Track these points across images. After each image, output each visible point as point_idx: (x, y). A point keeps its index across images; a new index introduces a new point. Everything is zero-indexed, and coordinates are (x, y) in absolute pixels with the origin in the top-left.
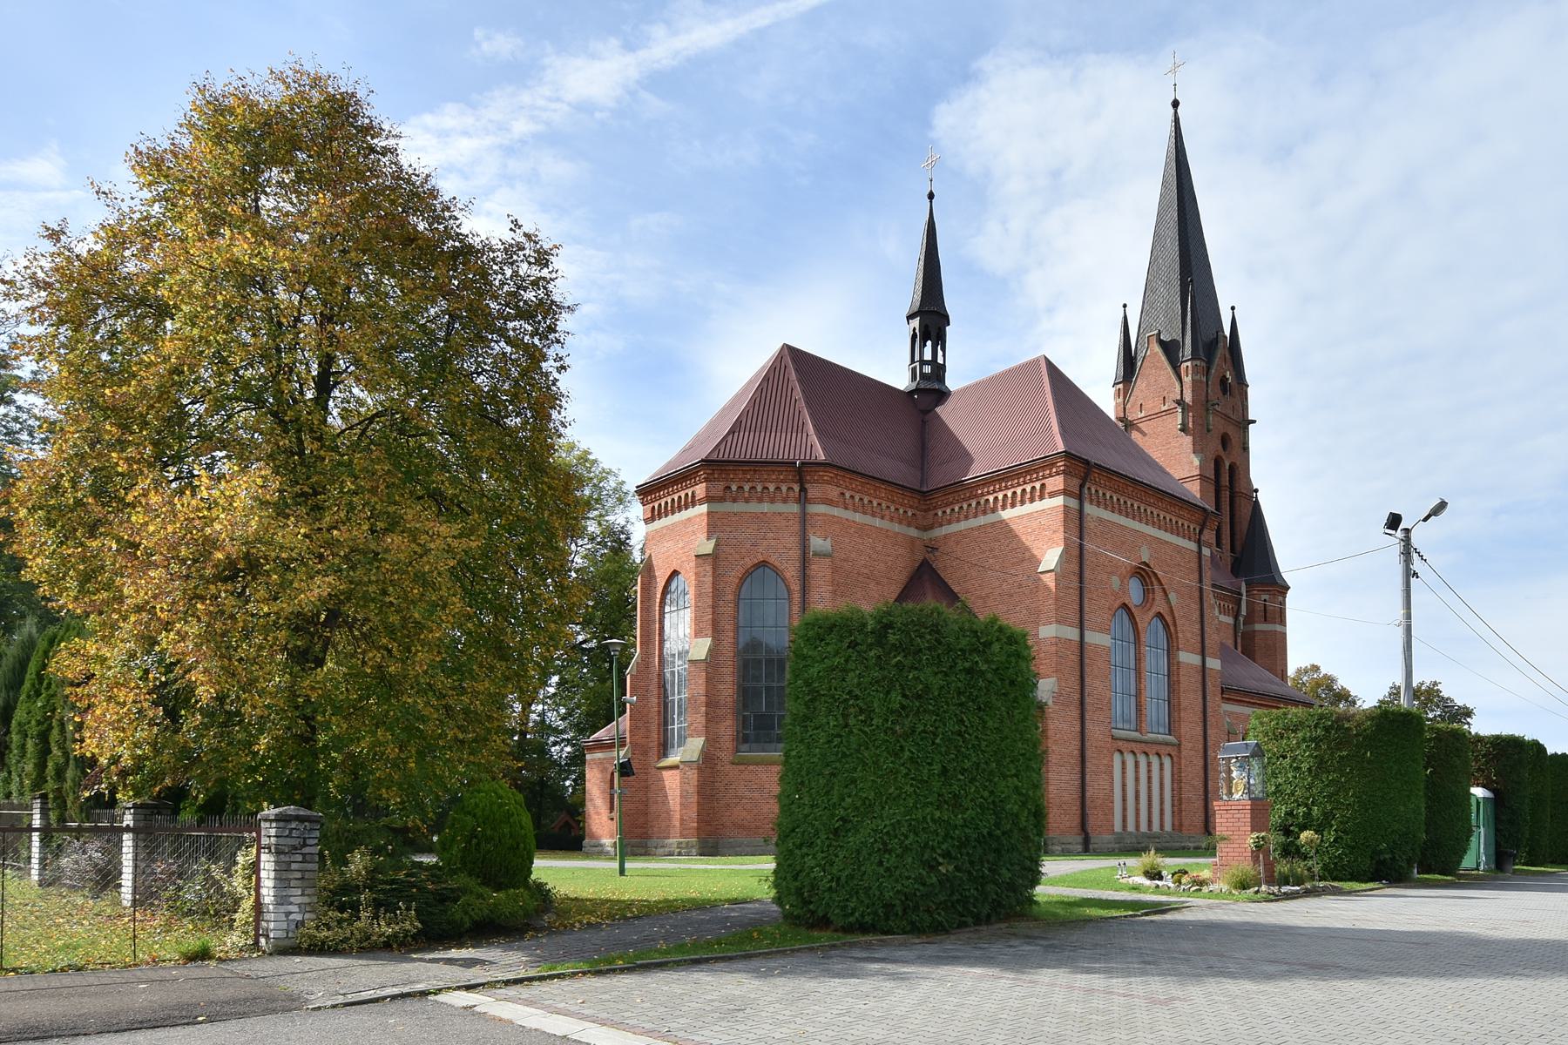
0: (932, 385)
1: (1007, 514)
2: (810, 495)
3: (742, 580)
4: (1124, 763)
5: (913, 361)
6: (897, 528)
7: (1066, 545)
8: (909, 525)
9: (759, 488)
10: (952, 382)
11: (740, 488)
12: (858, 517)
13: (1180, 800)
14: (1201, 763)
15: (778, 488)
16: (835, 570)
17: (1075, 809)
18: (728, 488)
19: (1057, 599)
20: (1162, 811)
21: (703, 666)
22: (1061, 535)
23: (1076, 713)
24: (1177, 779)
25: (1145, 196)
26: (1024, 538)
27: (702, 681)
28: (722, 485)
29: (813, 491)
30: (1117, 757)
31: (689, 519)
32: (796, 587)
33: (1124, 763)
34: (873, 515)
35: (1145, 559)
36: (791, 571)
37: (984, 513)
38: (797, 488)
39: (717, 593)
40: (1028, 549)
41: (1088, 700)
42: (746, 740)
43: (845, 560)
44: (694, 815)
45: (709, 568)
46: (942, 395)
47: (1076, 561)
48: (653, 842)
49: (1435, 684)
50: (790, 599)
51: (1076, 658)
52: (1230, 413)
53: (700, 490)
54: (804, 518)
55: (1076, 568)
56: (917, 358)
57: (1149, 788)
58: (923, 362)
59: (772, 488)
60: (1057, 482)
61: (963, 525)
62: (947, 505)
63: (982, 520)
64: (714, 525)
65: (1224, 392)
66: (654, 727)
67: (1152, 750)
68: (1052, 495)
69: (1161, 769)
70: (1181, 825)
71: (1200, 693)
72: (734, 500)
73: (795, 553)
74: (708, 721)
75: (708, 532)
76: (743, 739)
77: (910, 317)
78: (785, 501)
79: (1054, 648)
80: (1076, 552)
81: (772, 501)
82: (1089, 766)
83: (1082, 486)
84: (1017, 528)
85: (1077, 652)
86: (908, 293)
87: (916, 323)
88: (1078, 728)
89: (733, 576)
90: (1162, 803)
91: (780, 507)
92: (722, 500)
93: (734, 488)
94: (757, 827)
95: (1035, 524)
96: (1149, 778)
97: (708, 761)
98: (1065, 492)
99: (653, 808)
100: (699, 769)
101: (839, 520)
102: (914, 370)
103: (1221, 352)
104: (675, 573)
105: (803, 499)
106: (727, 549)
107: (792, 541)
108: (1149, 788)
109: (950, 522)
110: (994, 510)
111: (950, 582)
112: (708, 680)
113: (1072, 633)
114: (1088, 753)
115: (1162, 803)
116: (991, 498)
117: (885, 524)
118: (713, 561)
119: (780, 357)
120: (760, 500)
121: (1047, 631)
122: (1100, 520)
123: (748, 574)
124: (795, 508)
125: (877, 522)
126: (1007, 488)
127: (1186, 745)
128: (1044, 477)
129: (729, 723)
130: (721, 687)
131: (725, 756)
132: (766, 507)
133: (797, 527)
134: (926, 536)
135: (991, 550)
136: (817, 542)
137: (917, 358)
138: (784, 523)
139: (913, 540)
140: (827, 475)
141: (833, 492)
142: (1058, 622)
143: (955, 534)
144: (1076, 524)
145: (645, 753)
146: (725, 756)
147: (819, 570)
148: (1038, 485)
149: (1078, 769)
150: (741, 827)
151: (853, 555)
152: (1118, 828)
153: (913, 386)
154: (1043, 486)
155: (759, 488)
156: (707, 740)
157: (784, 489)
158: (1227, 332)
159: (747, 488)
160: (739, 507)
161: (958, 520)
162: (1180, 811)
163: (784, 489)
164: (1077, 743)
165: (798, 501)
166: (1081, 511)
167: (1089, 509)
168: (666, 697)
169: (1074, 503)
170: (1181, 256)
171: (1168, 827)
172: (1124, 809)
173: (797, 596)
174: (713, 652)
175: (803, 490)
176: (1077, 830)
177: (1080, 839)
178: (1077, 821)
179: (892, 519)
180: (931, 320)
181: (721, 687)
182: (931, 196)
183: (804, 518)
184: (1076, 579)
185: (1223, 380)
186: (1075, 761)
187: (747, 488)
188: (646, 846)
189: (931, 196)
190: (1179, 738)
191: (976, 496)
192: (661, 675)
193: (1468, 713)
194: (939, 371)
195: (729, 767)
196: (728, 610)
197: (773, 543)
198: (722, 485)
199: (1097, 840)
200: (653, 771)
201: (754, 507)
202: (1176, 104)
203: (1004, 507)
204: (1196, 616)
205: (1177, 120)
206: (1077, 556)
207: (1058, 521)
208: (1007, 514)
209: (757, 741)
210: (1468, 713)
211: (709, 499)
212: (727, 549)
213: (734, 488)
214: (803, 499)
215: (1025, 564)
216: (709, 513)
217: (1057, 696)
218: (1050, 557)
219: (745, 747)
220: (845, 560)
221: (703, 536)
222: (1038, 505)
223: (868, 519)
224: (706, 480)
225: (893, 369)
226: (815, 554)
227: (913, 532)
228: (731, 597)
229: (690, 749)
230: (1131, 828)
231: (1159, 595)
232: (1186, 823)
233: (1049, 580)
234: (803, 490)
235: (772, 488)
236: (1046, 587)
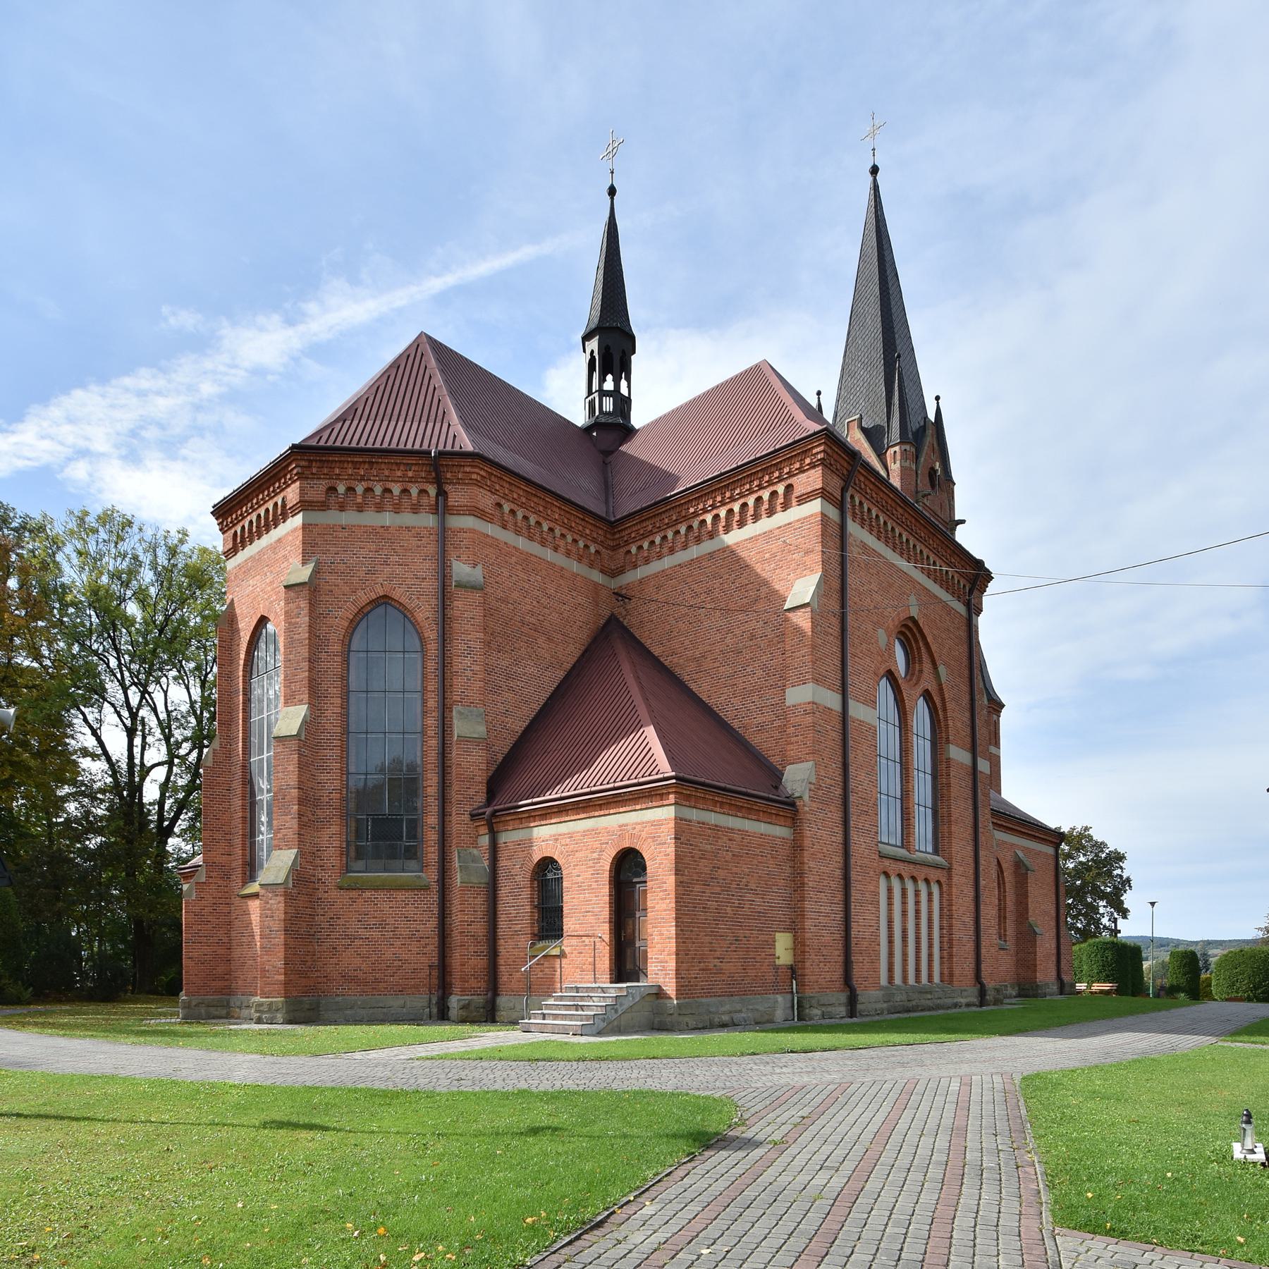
0: (613, 426)
1: (732, 538)
2: (452, 501)
3: (354, 625)
4: (890, 890)
5: (590, 392)
6: (575, 567)
7: (825, 571)
8: (591, 566)
9: (378, 490)
10: (638, 419)
11: (351, 489)
12: (521, 543)
13: (950, 941)
14: (972, 894)
15: (405, 491)
16: (488, 612)
17: (837, 955)
18: (332, 489)
19: (814, 647)
20: (930, 955)
21: (294, 745)
22: (817, 557)
23: (837, 816)
24: (947, 913)
25: (846, 252)
26: (758, 568)
27: (292, 767)
28: (323, 485)
29: (457, 496)
30: (882, 880)
31: (279, 540)
32: (431, 634)
33: (890, 890)
34: (543, 543)
35: (914, 612)
36: (425, 612)
37: (698, 540)
38: (432, 491)
39: (316, 642)
40: (765, 583)
41: (852, 798)
42: (360, 854)
43: (505, 601)
44: (280, 964)
45: (304, 604)
46: (628, 432)
47: (836, 596)
48: (235, 1001)
49: (1086, 829)
50: (423, 651)
51: (836, 736)
52: (937, 509)
53: (292, 494)
54: (443, 536)
55: (836, 607)
56: (595, 387)
57: (917, 925)
58: (603, 393)
59: (396, 489)
60: (812, 479)
61: (667, 562)
62: (644, 537)
63: (695, 551)
64: (311, 543)
65: (933, 486)
66: (238, 841)
67: (921, 873)
68: (803, 499)
69: (930, 900)
70: (951, 975)
71: (970, 802)
72: (342, 508)
73: (431, 586)
74: (302, 825)
75: (304, 553)
76: (356, 852)
77: (586, 338)
78: (415, 509)
79: (809, 719)
80: (836, 584)
81: (397, 509)
82: (855, 895)
83: (844, 490)
84: (748, 555)
85: (839, 727)
86: (583, 305)
87: (593, 345)
88: (840, 838)
89: (340, 617)
90: (930, 946)
91: (407, 519)
92: (323, 506)
93: (341, 489)
94: (377, 981)
95: (775, 546)
96: (917, 912)
97: (301, 883)
98: (824, 494)
99: (236, 953)
100: (286, 895)
101: (494, 543)
102: (592, 404)
103: (929, 439)
104: (263, 621)
105: (442, 507)
106: (331, 578)
107: (426, 568)
108: (917, 925)
109: (647, 561)
110: (712, 535)
111: (648, 643)
112: (302, 766)
113: (832, 700)
114: (853, 875)
115: (930, 946)
116: (709, 518)
117: (559, 559)
118: (310, 593)
119: (416, 345)
120: (380, 508)
121: (799, 695)
122: (864, 546)
123: (362, 614)
124: (428, 520)
125: (548, 554)
126: (733, 499)
127: (958, 869)
128: (791, 475)
129: (334, 829)
130: (323, 777)
131: (330, 877)
132: (387, 519)
133: (432, 549)
134: (614, 584)
135: (709, 592)
136: (461, 569)
137: (595, 387)
138: (414, 542)
139: (596, 585)
140: (477, 473)
141: (486, 500)
142: (816, 681)
143: (656, 575)
144: (836, 538)
145: (226, 876)
146: (330, 877)
147: (465, 609)
148: (780, 488)
149: (839, 897)
150: (354, 980)
151: (515, 595)
152: (884, 981)
153: (593, 420)
154: (789, 488)
155: (378, 490)
156: (301, 854)
157: (414, 492)
158: (932, 416)
159: (360, 489)
160: (349, 518)
161: (660, 557)
162: (951, 956)
163: (414, 492)
164: (838, 859)
165: (435, 510)
166: (843, 527)
167: (853, 527)
168: (253, 794)
169: (833, 513)
170: (884, 333)
171: (936, 979)
172: (891, 954)
173: (433, 648)
174: (308, 725)
175: (442, 493)
176: (839, 984)
177: (843, 997)
178: (838, 973)
179: (568, 554)
180: (613, 345)
181: (323, 777)
182: (612, 191)
183: (443, 536)
184: (835, 622)
185: (932, 472)
186: (837, 884)
187: (360, 489)
188: (228, 1006)
189: (612, 191)
190: (949, 859)
191: (687, 518)
192: (246, 767)
193: (1119, 857)
194: (623, 404)
195: (335, 893)
196: (332, 665)
197: (399, 570)
198: (323, 485)
199: (869, 997)
200: (237, 901)
201: (371, 518)
202: (874, 170)
203: (728, 529)
204: (965, 700)
205: (876, 188)
206: (838, 585)
207: (812, 539)
208: (732, 538)
209: (377, 856)
210: (1119, 857)
211: (305, 505)
212: (331, 578)
213: (341, 489)
214: (442, 507)
215: (760, 606)
216: (305, 527)
217: (816, 788)
218: (802, 588)
219: (360, 864)
220: (505, 601)
221: (296, 560)
222: (781, 518)
223: (534, 548)
224: (301, 476)
225: (567, 393)
226: (459, 585)
227: (597, 577)
228: (337, 648)
229: (277, 864)
230: (898, 980)
231: (927, 666)
232: (957, 972)
233: (803, 621)
234: (442, 493)
235: (396, 489)
236: (798, 630)
